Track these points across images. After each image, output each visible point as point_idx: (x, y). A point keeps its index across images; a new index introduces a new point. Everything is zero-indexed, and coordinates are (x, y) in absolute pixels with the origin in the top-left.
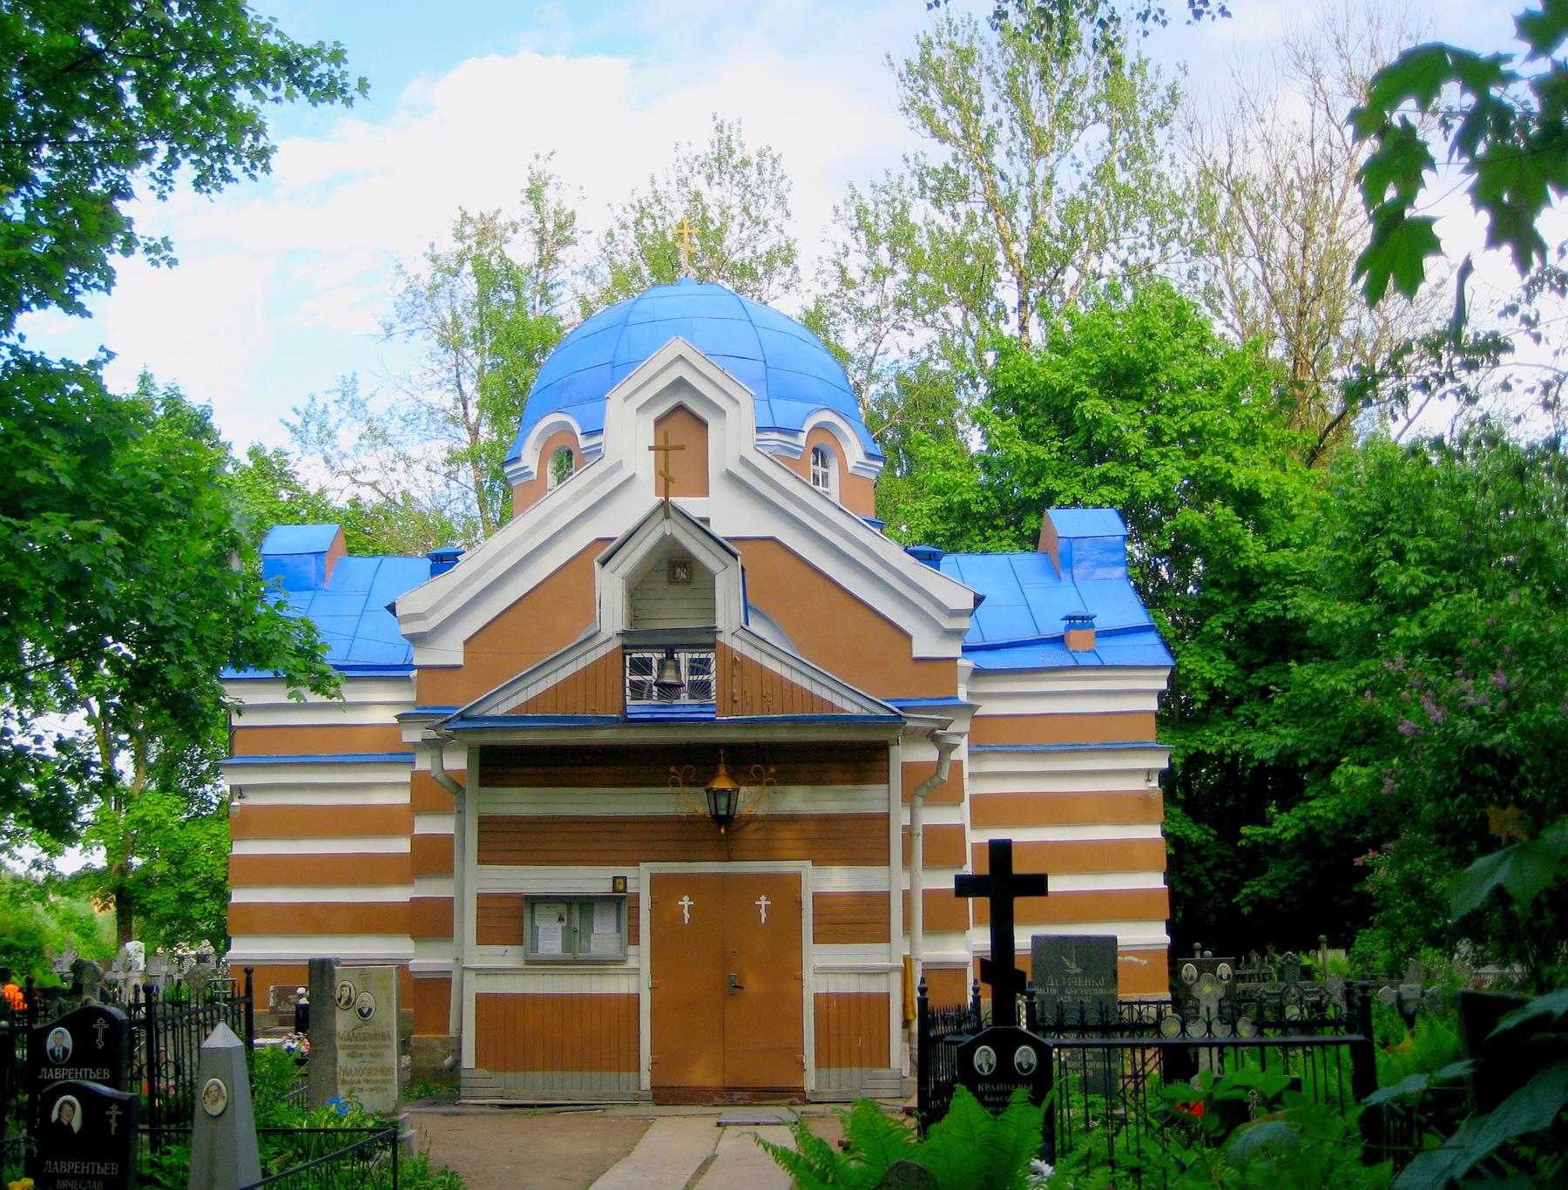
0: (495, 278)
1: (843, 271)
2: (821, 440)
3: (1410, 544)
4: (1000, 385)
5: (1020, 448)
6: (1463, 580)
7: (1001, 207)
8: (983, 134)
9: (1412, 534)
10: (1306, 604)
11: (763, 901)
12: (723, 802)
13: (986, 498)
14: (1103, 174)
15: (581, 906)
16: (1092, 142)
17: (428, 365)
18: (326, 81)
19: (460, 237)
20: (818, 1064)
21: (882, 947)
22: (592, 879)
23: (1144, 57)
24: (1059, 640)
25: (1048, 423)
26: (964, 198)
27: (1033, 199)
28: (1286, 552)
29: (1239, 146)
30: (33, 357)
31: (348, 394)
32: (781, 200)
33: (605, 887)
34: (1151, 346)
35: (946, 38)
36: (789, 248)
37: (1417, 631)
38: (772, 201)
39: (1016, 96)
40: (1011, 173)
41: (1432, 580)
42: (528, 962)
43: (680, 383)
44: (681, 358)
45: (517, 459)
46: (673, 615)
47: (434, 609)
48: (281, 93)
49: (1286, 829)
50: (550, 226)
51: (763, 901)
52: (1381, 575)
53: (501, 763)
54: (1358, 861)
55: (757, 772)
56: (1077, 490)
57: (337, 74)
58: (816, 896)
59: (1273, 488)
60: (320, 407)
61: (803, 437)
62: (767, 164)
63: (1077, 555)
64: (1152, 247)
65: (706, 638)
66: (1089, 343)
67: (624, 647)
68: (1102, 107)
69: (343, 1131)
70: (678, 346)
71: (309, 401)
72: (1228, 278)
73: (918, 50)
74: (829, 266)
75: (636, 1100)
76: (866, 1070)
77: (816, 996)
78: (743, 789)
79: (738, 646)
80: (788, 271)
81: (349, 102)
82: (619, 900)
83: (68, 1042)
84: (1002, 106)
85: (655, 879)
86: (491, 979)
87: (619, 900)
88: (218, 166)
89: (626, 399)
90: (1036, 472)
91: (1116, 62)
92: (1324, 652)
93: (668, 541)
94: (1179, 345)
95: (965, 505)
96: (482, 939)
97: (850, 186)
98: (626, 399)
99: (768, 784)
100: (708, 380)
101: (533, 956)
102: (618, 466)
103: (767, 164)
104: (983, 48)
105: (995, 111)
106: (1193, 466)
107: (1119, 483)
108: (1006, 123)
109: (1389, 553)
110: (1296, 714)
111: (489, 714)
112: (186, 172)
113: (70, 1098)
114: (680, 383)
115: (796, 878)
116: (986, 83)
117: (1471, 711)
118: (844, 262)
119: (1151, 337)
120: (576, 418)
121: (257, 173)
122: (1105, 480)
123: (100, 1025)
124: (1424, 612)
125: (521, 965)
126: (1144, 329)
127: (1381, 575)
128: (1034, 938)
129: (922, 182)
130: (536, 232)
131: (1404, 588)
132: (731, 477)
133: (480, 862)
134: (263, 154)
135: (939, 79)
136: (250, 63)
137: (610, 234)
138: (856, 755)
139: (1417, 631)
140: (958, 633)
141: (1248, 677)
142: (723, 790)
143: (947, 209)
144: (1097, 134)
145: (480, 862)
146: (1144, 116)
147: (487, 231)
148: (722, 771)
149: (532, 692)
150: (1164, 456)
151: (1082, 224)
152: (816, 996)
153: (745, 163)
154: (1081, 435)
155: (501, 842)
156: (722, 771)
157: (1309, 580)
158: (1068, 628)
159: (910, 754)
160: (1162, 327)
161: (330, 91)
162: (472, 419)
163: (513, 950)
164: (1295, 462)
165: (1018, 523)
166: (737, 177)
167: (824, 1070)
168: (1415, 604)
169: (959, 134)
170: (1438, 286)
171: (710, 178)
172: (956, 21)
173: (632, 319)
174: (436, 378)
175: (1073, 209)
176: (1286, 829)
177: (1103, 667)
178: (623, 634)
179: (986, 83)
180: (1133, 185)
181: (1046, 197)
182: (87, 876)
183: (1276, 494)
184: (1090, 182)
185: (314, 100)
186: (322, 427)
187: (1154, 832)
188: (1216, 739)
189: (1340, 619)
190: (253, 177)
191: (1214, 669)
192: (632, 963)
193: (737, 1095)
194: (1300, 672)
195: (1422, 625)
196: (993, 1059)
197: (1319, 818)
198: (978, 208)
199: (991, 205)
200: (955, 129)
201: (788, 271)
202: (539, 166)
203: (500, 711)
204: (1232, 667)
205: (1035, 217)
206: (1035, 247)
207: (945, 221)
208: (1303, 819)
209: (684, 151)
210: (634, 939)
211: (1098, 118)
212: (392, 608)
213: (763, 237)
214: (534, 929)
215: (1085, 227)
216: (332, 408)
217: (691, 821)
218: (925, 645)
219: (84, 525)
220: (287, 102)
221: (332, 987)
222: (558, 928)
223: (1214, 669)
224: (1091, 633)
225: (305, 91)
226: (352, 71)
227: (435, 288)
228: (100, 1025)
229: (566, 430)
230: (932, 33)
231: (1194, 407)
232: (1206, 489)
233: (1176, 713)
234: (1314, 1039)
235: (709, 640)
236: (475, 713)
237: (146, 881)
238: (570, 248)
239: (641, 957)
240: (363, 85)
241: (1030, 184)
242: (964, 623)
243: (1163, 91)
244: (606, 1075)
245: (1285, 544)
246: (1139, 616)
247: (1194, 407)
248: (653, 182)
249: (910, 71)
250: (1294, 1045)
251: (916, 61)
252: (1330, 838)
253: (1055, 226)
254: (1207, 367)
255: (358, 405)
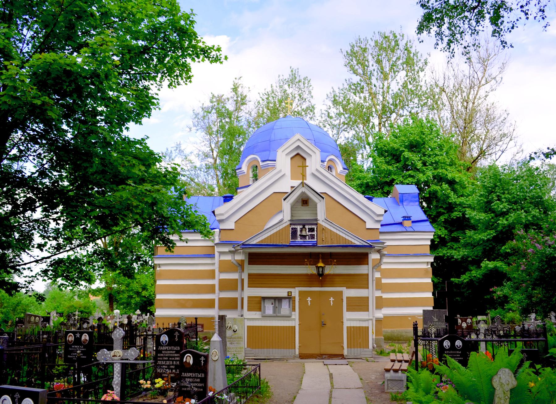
0: (222, 114)
1: (329, 113)
2: (331, 164)
3: (503, 196)
4: (379, 147)
5: (384, 167)
6: (519, 207)
7: (373, 95)
8: (369, 73)
9: (504, 193)
10: (469, 213)
11: (332, 299)
12: (321, 270)
13: (373, 181)
14: (405, 86)
15: (279, 299)
16: (402, 76)
17: (202, 139)
18: (215, 56)
19: (212, 102)
20: (348, 347)
21: (366, 313)
22: (282, 292)
23: (417, 51)
24: (401, 224)
25: (392, 159)
26: (362, 92)
27: (383, 92)
28: (463, 198)
29: (447, 77)
30: (125, 137)
31: (178, 147)
32: (310, 92)
33: (285, 295)
34: (424, 136)
35: (358, 45)
36: (313, 107)
37: (506, 222)
38: (307, 93)
39: (379, 62)
40: (377, 85)
41: (510, 207)
42: (263, 317)
43: (298, 147)
44: (299, 139)
45: (240, 168)
46: (304, 214)
47: (227, 212)
48: (200, 60)
49: (465, 279)
50: (239, 99)
51: (332, 299)
52: (494, 205)
53: (255, 258)
54: (491, 290)
55: (331, 261)
56: (401, 179)
57: (218, 54)
58: (347, 298)
59: (459, 179)
60: (170, 152)
61: (326, 163)
62: (306, 82)
63: (404, 199)
64: (419, 107)
65: (315, 222)
66: (405, 135)
67: (291, 224)
68: (405, 66)
69: (234, 365)
70: (298, 136)
71: (166, 150)
72: (439, 116)
73: (350, 48)
74: (325, 112)
75: (295, 357)
76: (362, 349)
77: (347, 327)
78: (326, 266)
79: (324, 224)
80: (312, 114)
81: (221, 63)
82: (290, 298)
83: (167, 339)
84: (375, 64)
85: (300, 293)
86: (251, 321)
87: (290, 298)
88: (176, 81)
89: (283, 151)
90: (390, 173)
91: (409, 52)
92: (474, 228)
93: (303, 193)
94: (431, 136)
95: (367, 184)
96: (249, 309)
97: (332, 88)
98: (283, 151)
99: (334, 265)
100: (307, 146)
101: (264, 315)
102: (280, 171)
103: (306, 82)
104: (370, 48)
105: (372, 66)
106: (436, 172)
107: (413, 177)
108: (376, 70)
109: (496, 198)
110: (465, 246)
111: (251, 243)
112: (166, 83)
113: (189, 355)
114: (298, 147)
115: (341, 292)
116: (370, 58)
117: (550, 246)
118: (329, 111)
119: (424, 134)
120: (249, 155)
121: (187, 83)
122: (410, 176)
123: (177, 334)
124: (507, 216)
125: (260, 317)
126: (422, 132)
127: (494, 205)
128: (424, 311)
129: (350, 86)
130: (235, 101)
131: (502, 209)
132: (313, 175)
133: (248, 287)
134: (190, 77)
135: (356, 57)
136: (192, 51)
137: (259, 102)
138: (358, 257)
139: (506, 222)
140: (379, 221)
141: (451, 234)
142: (321, 267)
143: (358, 95)
144: (403, 74)
145: (248, 287)
146: (417, 68)
147: (220, 100)
148: (321, 261)
149: (264, 237)
150: (427, 169)
151: (398, 101)
152: (347, 327)
153: (300, 81)
154: (402, 163)
155: (256, 280)
156: (321, 261)
157: (470, 207)
158: (404, 220)
159: (374, 256)
160: (426, 131)
161: (217, 59)
162: (215, 156)
163: (258, 313)
164: (464, 172)
165: (382, 189)
166: (297, 85)
167: (349, 349)
168: (504, 214)
169: (362, 73)
170: (504, 120)
171: (289, 85)
172: (362, 40)
173: (275, 127)
174: (204, 143)
175: (396, 96)
176: (465, 279)
177: (414, 232)
178: (290, 221)
179: (370, 58)
180: (413, 89)
181: (388, 92)
182: (99, 290)
183: (460, 181)
184: (401, 88)
185: (211, 62)
186: (170, 157)
187: (429, 281)
188: (443, 252)
189: (482, 218)
190: (186, 84)
191: (443, 232)
192: (293, 317)
193: (324, 356)
194: (469, 233)
195: (507, 220)
196: (449, 344)
197: (475, 276)
198: (367, 95)
199: (371, 94)
200: (360, 71)
201: (312, 114)
202: (236, 81)
203: (254, 243)
204: (446, 231)
205: (384, 98)
206: (384, 107)
207: (357, 99)
208: (470, 277)
209: (281, 78)
210: (294, 310)
211: (403, 69)
212: (213, 212)
213: (304, 103)
214: (264, 307)
215: (400, 101)
216: (173, 152)
217: (312, 275)
218: (370, 224)
219: (156, 187)
220: (201, 62)
221: (225, 324)
222: (271, 307)
223: (443, 232)
224: (411, 221)
225: (209, 60)
226: (223, 53)
227: (204, 117)
228: (177, 334)
229: (255, 159)
230: (354, 43)
231: (437, 155)
232: (440, 179)
233: (434, 246)
234: (509, 339)
235: (316, 222)
236: (247, 243)
237: (119, 292)
238: (245, 106)
239: (296, 315)
240: (226, 58)
241: (383, 88)
242: (381, 218)
243: (423, 61)
244: (285, 350)
245: (462, 196)
246: (424, 217)
247: (437, 155)
248: (272, 87)
249: (348, 54)
250: (504, 341)
251: (349, 51)
252: (477, 282)
253: (391, 101)
254: (439, 143)
255: (181, 151)
